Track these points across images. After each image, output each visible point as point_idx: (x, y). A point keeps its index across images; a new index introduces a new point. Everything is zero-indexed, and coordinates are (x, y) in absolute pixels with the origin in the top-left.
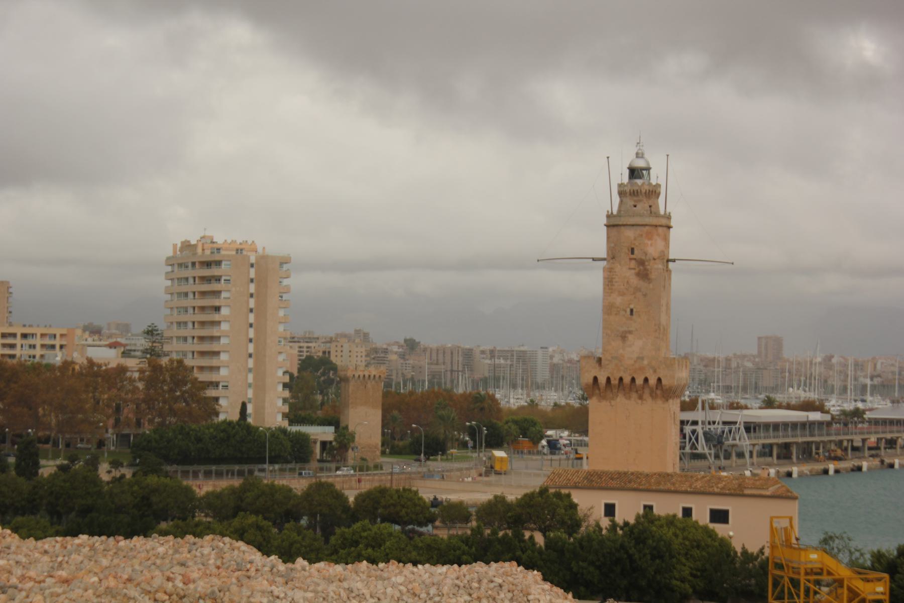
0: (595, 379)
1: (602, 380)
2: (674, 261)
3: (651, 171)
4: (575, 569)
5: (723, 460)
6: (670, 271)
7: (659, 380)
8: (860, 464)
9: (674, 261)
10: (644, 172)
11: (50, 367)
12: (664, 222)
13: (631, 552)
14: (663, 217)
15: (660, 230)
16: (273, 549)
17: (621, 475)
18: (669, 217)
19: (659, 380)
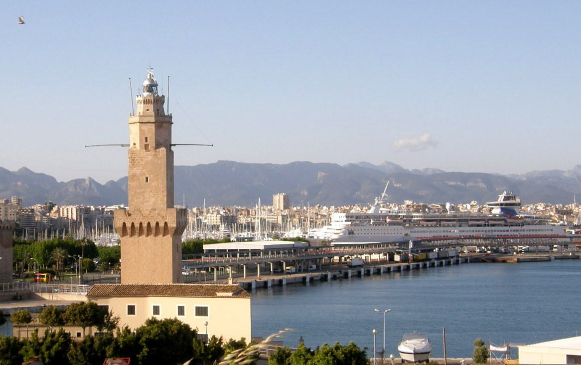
0: (124, 224)
1: (129, 225)
2: (175, 145)
3: (158, 87)
4: (557, 207)
5: (256, 233)
6: (173, 152)
7: (166, 223)
8: (326, 273)
9: (175, 145)
10: (154, 88)
11: (193, 349)
12: (167, 119)
13: (482, 240)
14: (167, 116)
15: (165, 125)
16: (109, 332)
17: (143, 287)
18: (170, 117)
19: (166, 223)
